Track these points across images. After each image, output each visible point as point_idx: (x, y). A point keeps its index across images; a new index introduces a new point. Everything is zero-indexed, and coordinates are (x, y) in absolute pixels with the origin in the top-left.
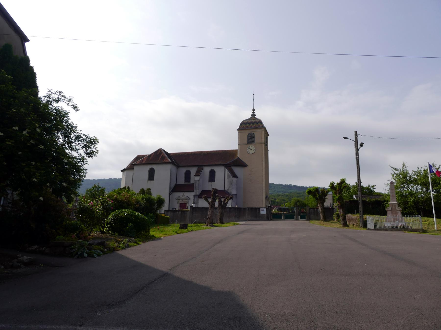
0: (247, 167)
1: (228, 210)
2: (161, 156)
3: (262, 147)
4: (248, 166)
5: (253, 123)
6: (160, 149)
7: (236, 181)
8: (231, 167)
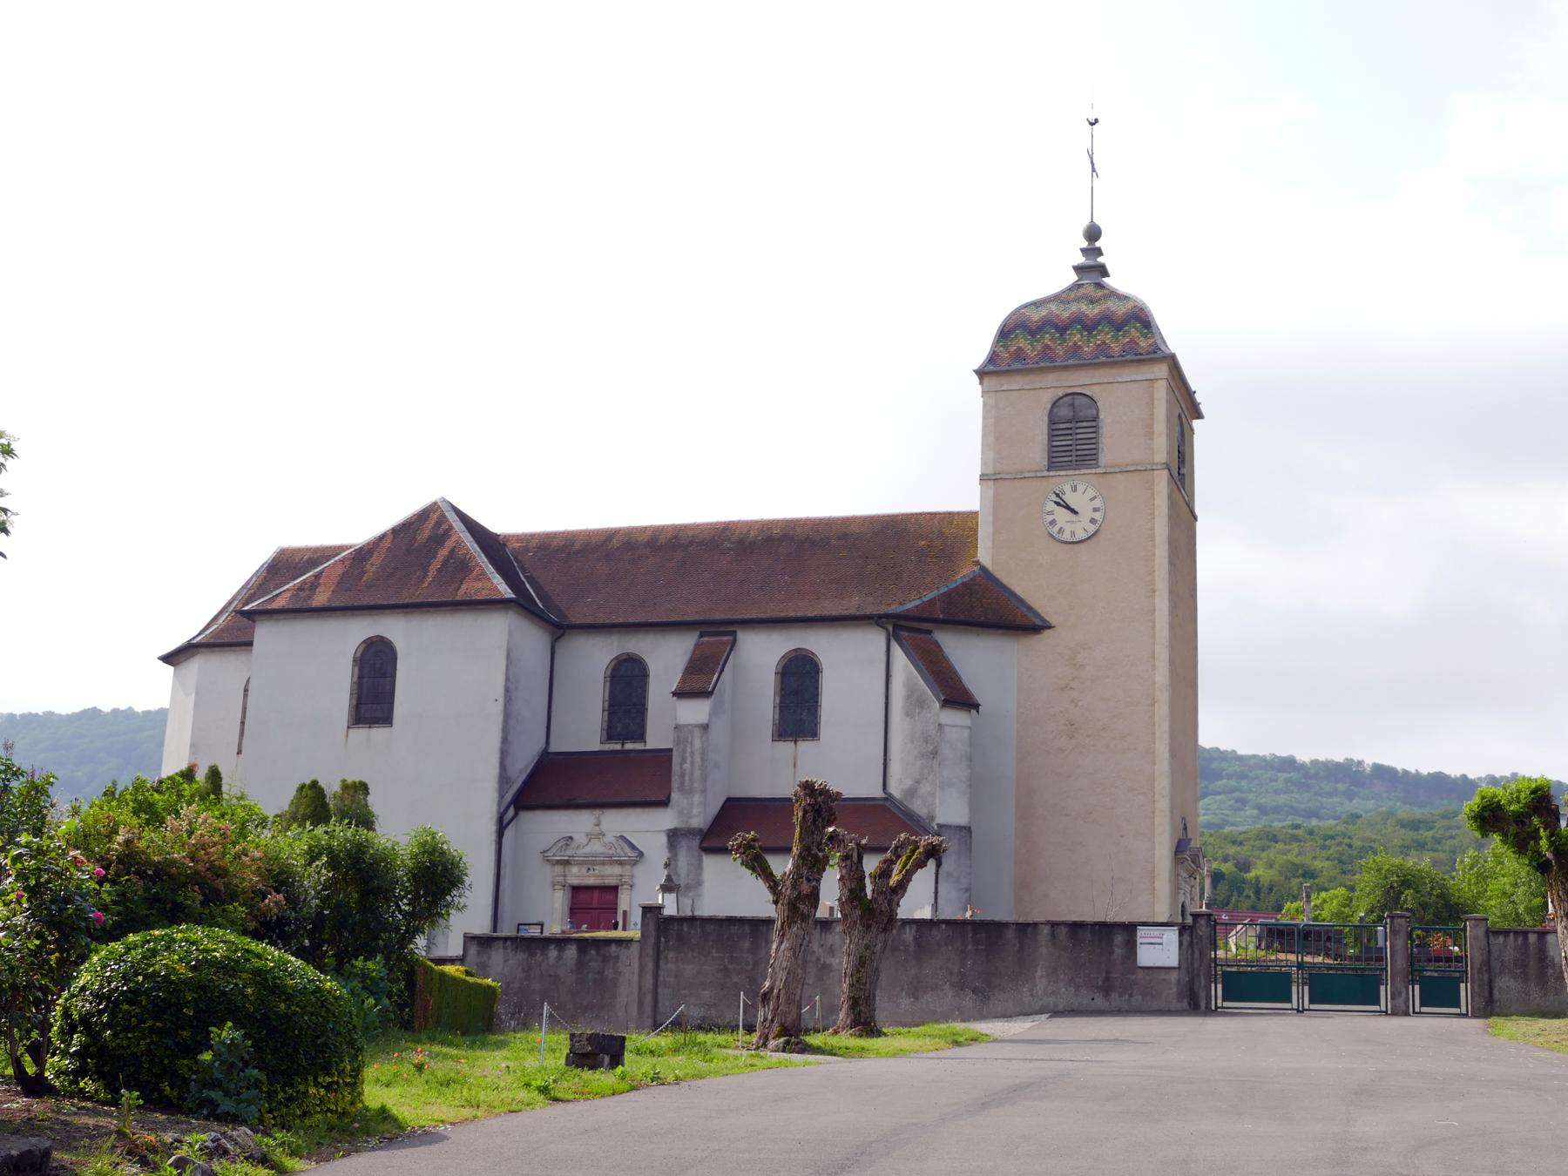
0: (1047, 633)
1: (909, 934)
2: (443, 553)
4: (1050, 627)
5: (1088, 326)
6: (435, 504)
7: (966, 733)
8: (930, 632)
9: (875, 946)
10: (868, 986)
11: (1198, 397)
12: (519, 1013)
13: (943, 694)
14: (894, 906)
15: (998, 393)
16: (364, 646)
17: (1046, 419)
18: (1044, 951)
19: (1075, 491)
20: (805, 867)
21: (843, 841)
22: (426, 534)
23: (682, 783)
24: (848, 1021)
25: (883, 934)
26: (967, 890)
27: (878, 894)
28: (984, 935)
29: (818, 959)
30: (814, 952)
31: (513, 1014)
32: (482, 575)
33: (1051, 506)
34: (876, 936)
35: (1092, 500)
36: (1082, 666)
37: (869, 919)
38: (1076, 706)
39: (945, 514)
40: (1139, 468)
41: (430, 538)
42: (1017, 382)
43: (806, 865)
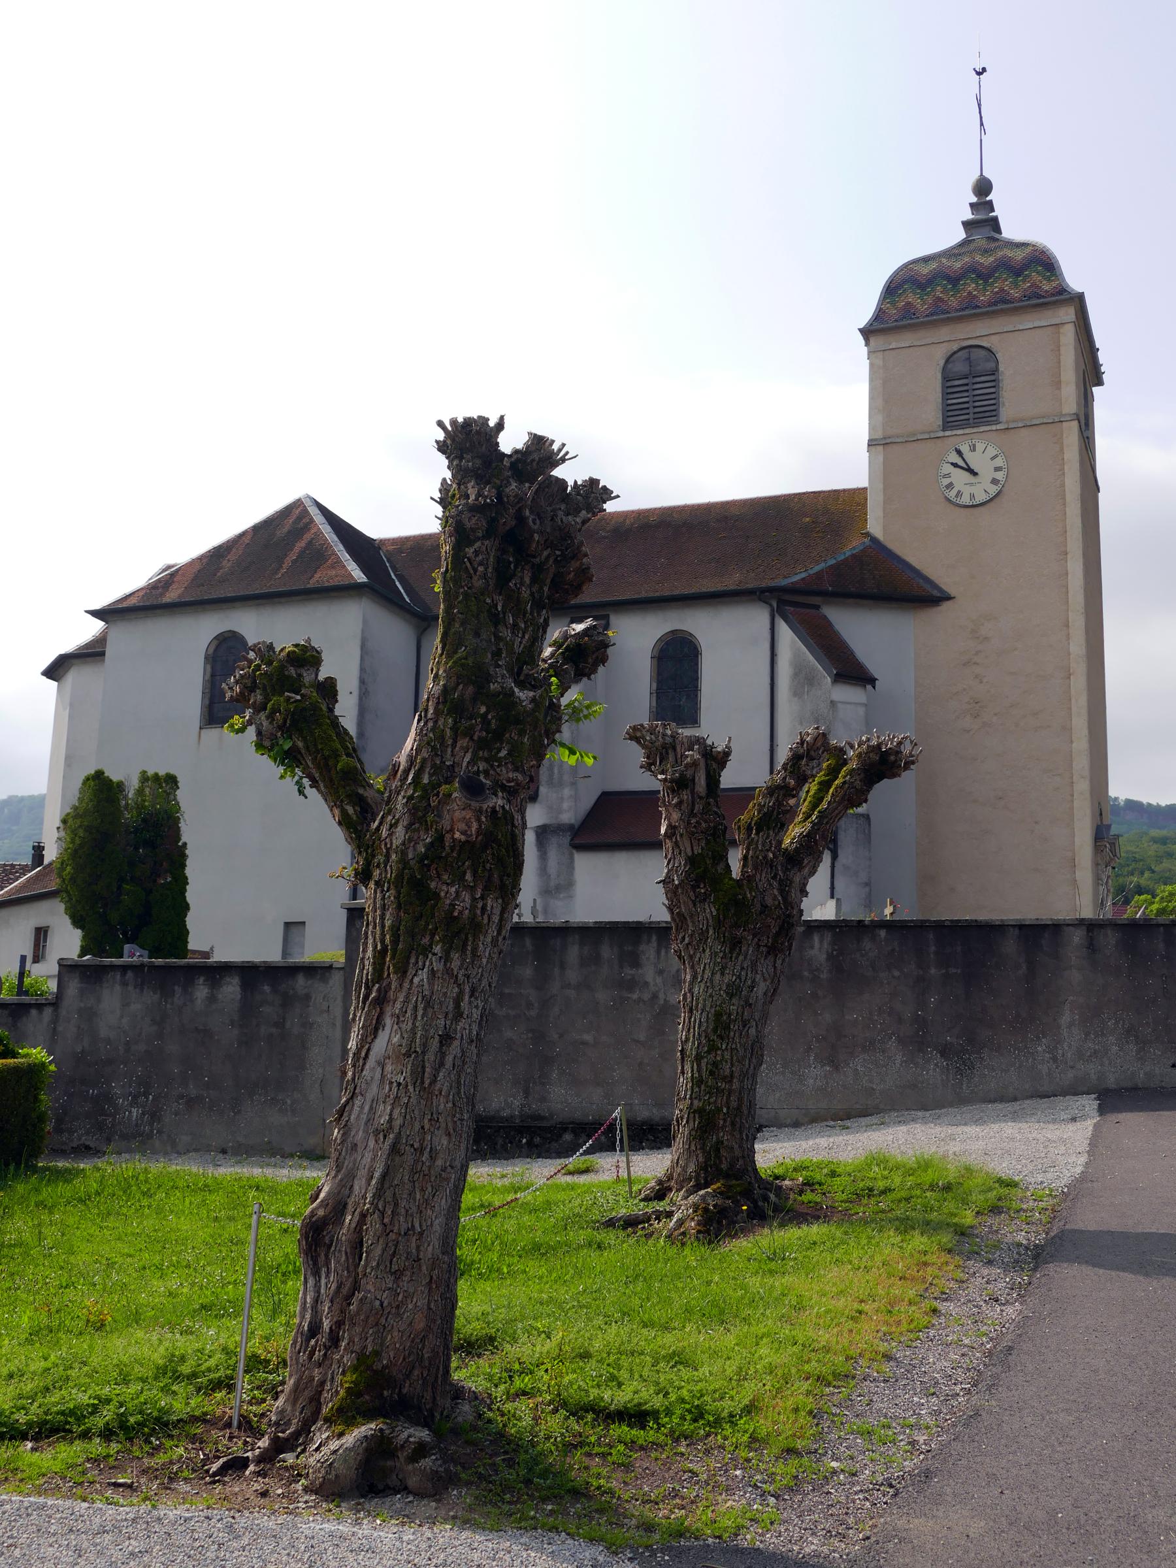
0: (946, 605)
1: (818, 950)
2: (301, 544)
3: (1062, 451)
4: (949, 598)
5: (984, 276)
6: (299, 500)
7: (861, 711)
8: (817, 607)
9: (752, 987)
10: (736, 1085)
11: (1102, 357)
12: (146, 1094)
13: (836, 668)
14: (793, 894)
15: (887, 352)
16: (216, 642)
17: (939, 376)
18: (1075, 976)
19: (974, 450)
20: (463, 742)
21: (674, 749)
22: (285, 530)
23: (551, 776)
24: (691, 1168)
25: (771, 958)
26: (867, 884)
27: (755, 868)
28: (959, 949)
29: (655, 996)
30: (646, 984)
31: (135, 1097)
32: (339, 563)
33: (948, 469)
34: (754, 965)
35: (993, 458)
36: (986, 639)
37: (736, 926)
38: (981, 682)
39: (829, 491)
40: (1045, 421)
41: (289, 532)
42: (906, 339)
43: (469, 732)
